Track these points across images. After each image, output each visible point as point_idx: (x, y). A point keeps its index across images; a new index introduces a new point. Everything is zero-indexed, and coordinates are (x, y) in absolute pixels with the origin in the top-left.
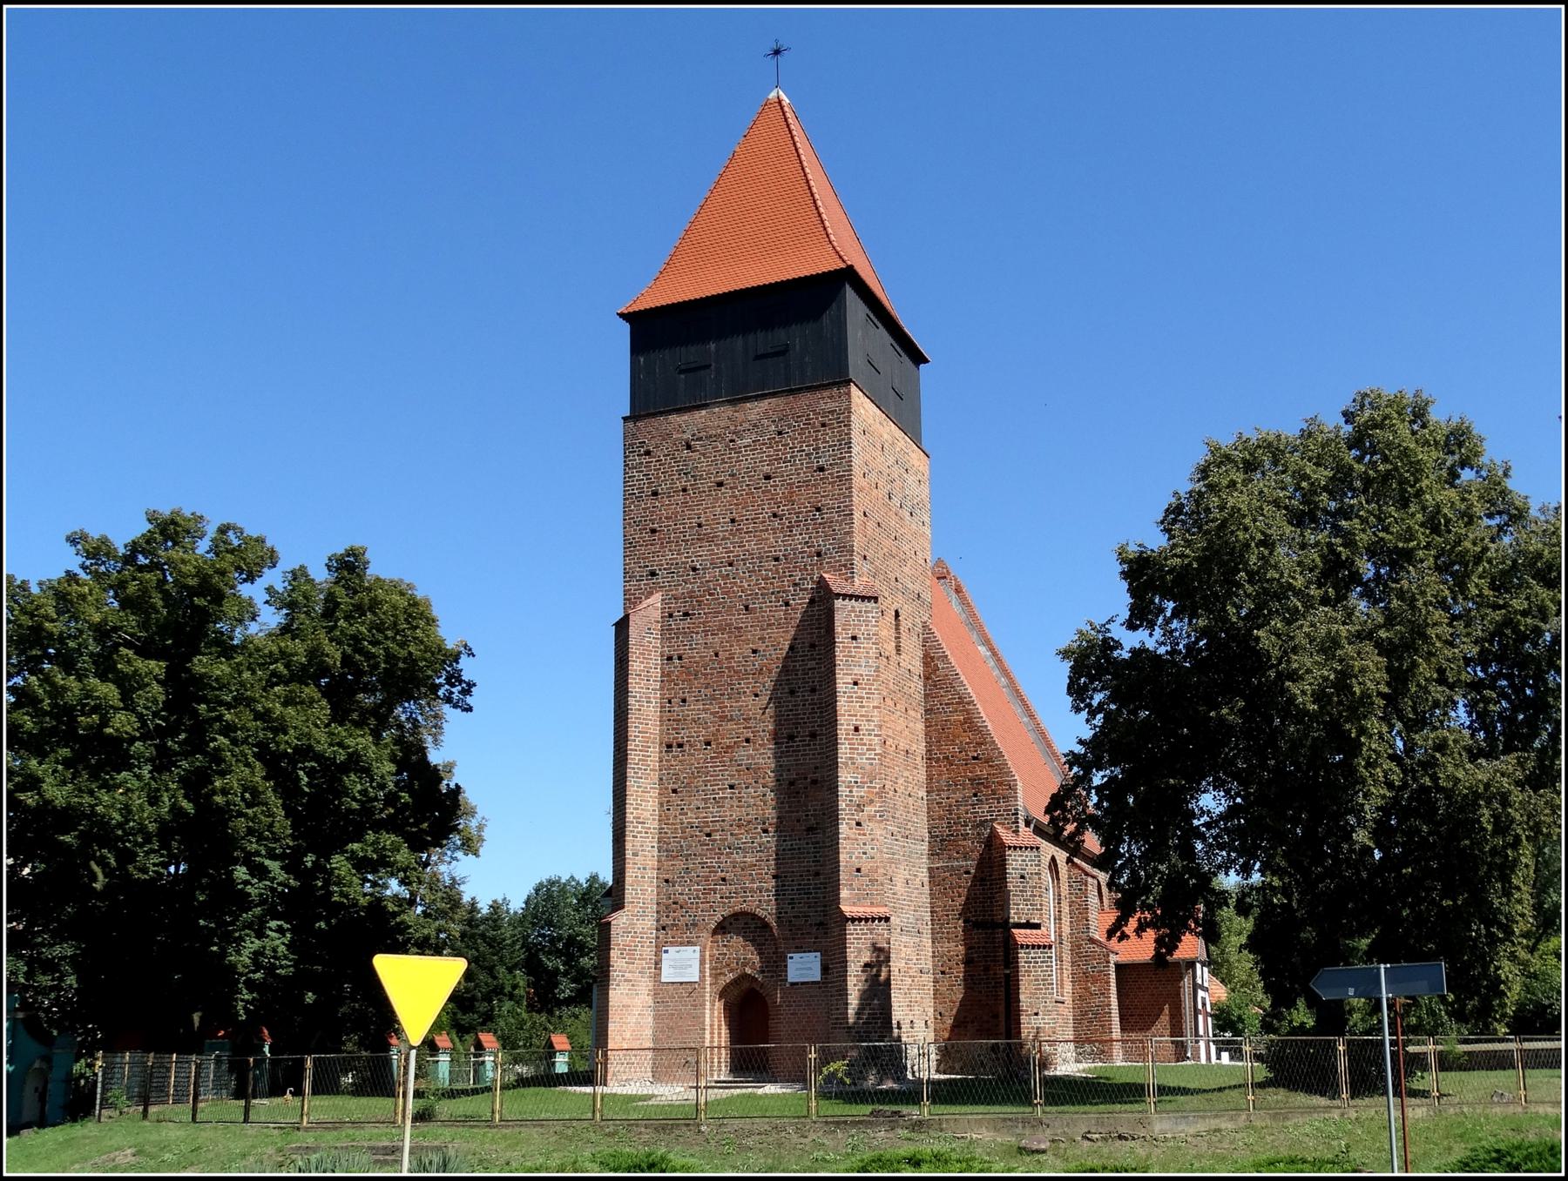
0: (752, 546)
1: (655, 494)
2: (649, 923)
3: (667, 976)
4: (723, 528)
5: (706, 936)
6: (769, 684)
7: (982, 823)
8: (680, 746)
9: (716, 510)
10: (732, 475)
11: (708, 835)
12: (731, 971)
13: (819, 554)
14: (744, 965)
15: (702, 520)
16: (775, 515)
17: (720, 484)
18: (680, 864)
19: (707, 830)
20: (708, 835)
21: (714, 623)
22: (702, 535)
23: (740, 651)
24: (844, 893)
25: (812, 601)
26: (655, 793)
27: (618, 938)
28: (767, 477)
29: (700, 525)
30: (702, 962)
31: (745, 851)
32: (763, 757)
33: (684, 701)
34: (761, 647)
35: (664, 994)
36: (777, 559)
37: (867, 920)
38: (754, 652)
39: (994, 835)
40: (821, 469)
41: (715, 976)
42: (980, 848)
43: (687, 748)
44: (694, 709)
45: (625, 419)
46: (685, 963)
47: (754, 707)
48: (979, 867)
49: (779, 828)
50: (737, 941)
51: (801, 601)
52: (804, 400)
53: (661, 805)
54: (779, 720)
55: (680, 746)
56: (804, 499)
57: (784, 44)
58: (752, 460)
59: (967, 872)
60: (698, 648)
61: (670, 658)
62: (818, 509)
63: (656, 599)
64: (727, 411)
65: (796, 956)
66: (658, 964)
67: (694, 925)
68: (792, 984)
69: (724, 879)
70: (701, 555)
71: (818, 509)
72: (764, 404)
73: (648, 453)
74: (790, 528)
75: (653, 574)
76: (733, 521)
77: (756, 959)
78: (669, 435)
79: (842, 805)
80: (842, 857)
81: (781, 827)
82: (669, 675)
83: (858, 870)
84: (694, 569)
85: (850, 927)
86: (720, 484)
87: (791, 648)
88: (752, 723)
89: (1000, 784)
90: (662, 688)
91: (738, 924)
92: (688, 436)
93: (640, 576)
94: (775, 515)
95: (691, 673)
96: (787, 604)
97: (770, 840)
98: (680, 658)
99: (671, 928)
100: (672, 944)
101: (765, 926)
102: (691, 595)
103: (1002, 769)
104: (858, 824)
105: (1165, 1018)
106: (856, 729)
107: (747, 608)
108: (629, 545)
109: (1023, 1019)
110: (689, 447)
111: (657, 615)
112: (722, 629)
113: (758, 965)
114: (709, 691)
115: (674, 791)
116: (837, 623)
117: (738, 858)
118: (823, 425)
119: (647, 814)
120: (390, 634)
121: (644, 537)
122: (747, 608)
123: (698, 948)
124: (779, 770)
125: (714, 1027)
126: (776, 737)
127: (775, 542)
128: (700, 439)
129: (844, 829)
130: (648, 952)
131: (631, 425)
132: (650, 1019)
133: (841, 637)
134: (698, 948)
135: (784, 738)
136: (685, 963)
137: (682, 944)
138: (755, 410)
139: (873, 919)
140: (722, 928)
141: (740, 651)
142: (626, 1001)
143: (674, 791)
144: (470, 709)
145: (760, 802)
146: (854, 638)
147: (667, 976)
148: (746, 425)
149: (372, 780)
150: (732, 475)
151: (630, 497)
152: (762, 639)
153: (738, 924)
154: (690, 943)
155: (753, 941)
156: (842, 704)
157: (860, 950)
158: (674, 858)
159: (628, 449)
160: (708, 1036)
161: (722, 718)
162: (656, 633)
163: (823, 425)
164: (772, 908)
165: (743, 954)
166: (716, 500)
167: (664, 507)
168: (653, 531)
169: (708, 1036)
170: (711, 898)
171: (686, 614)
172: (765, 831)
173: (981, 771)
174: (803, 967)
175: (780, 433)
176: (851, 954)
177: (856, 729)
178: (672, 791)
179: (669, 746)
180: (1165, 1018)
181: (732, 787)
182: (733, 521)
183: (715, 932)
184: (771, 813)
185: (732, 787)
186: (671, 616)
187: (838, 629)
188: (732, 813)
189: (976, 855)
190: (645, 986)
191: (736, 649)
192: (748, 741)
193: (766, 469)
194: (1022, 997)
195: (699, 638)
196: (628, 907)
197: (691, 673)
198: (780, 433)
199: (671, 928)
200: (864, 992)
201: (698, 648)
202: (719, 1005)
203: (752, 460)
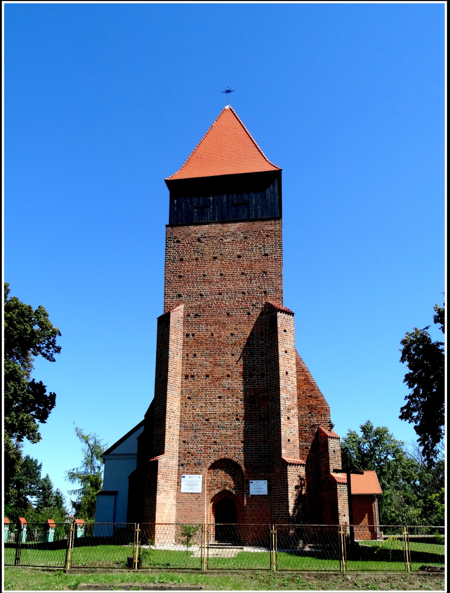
0: (231, 286)
1: (181, 260)
2: (175, 462)
3: (184, 489)
4: (216, 278)
5: (205, 470)
6: (240, 350)
7: (314, 426)
8: (193, 376)
9: (213, 269)
10: (221, 254)
11: (207, 420)
12: (218, 488)
13: (265, 292)
14: (225, 485)
15: (206, 273)
16: (243, 274)
17: (215, 258)
18: (192, 434)
19: (207, 418)
20: (207, 420)
21: (211, 320)
22: (205, 279)
23: (225, 333)
24: (283, 451)
25: (262, 314)
26: (179, 398)
27: (161, 469)
28: (239, 257)
29: (204, 275)
30: (203, 483)
31: (226, 428)
32: (238, 384)
33: (195, 355)
34: (236, 332)
35: (181, 498)
36: (244, 293)
37: (295, 465)
38: (232, 334)
39: (320, 431)
40: (266, 255)
41: (210, 491)
42: (313, 437)
43: (196, 378)
44: (200, 359)
45: (167, 226)
46: (194, 483)
47: (233, 361)
48: (312, 446)
49: (245, 418)
50: (222, 473)
51: (256, 313)
52: (258, 225)
53: (182, 404)
54: (245, 367)
55: (193, 376)
56: (257, 267)
57: (231, 88)
58: (230, 249)
59: (307, 448)
60: (203, 331)
61: (188, 335)
62: (265, 272)
63: (182, 307)
64: (220, 226)
65: (255, 482)
66: (179, 483)
67: (199, 464)
68: (252, 496)
69: (215, 442)
70: (205, 289)
71: (265, 272)
72: (238, 225)
73: (178, 242)
74: (251, 280)
75: (180, 296)
76: (221, 275)
77: (232, 482)
78: (190, 234)
79: (282, 408)
80: (283, 433)
81: (247, 417)
82: (187, 343)
83: (289, 441)
84: (201, 295)
85: (289, 468)
86: (215, 258)
87: (251, 334)
88: (231, 368)
89: (322, 408)
90: (183, 349)
91: (222, 464)
92: (199, 235)
93: (173, 296)
94: (243, 274)
95: (199, 343)
96: (249, 314)
97: (241, 424)
98: (193, 335)
99: (187, 465)
100: (187, 473)
101: (239, 467)
102: (199, 306)
103: (323, 402)
104: (288, 418)
105: (366, 520)
106: (287, 373)
107: (228, 314)
108: (167, 282)
109: (340, 518)
110: (199, 240)
111: (182, 314)
112: (215, 323)
113: (233, 485)
114: (208, 352)
115: (189, 398)
116: (278, 323)
117: (223, 432)
118: (267, 236)
119: (175, 408)
120: (27, 319)
121: (176, 280)
122: (228, 314)
123: (201, 476)
124: (245, 391)
125: (208, 517)
126: (244, 375)
127: (243, 285)
128: (205, 237)
129: (283, 420)
130: (174, 477)
131: (170, 229)
132: (175, 511)
133: (280, 330)
134: (201, 476)
135: (248, 374)
136: (194, 483)
137: (192, 473)
138: (233, 227)
139: (298, 465)
140: (214, 467)
141: (225, 333)
142: (164, 501)
143: (189, 398)
144: (54, 361)
145: (235, 405)
146: (285, 331)
147: (184, 489)
148: (229, 233)
149: (20, 386)
150: (221, 254)
151: (168, 260)
152: (236, 329)
153: (222, 464)
154: (196, 473)
155: (230, 474)
156: (281, 361)
157: (293, 480)
158: (188, 430)
159: (168, 239)
160: (205, 521)
161: (216, 365)
162: (182, 322)
163: (267, 236)
164: (242, 457)
165: (225, 479)
166: (213, 265)
167: (186, 266)
168: (180, 277)
169: (205, 521)
170: (208, 451)
171: (197, 315)
172: (238, 419)
173: (313, 402)
174: (259, 487)
175: (245, 238)
176: (290, 482)
177: (287, 373)
178: (188, 398)
179: (187, 377)
180: (366, 520)
181: (220, 397)
182: (221, 275)
183: (210, 468)
184: (241, 412)
185: (220, 397)
186: (189, 315)
187: (279, 326)
188: (219, 409)
189: (311, 440)
190: (173, 494)
191: (222, 333)
192: (228, 376)
193: (239, 253)
194: (339, 507)
195: (203, 327)
196: (166, 453)
197: (199, 343)
198: (245, 238)
199: (187, 465)
200: (296, 500)
201: (203, 331)
202: (211, 505)
203: (230, 249)
